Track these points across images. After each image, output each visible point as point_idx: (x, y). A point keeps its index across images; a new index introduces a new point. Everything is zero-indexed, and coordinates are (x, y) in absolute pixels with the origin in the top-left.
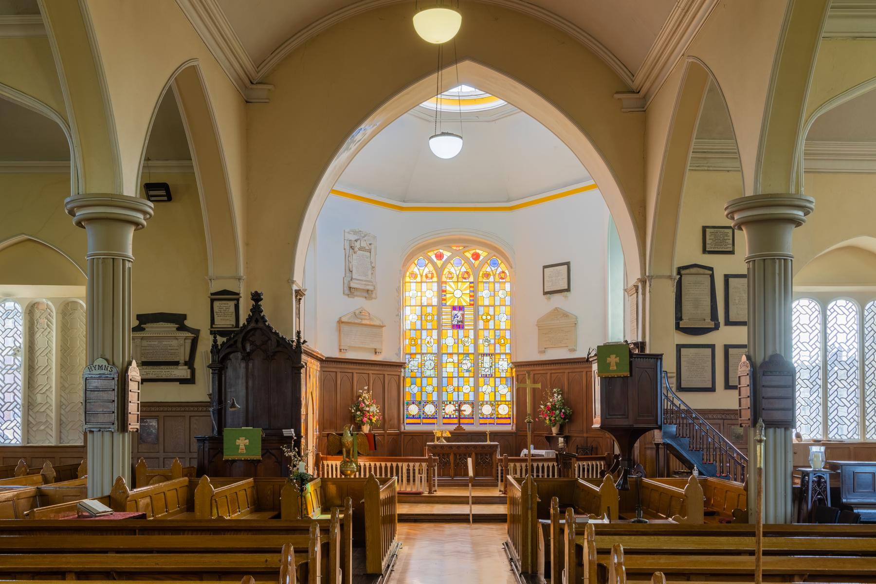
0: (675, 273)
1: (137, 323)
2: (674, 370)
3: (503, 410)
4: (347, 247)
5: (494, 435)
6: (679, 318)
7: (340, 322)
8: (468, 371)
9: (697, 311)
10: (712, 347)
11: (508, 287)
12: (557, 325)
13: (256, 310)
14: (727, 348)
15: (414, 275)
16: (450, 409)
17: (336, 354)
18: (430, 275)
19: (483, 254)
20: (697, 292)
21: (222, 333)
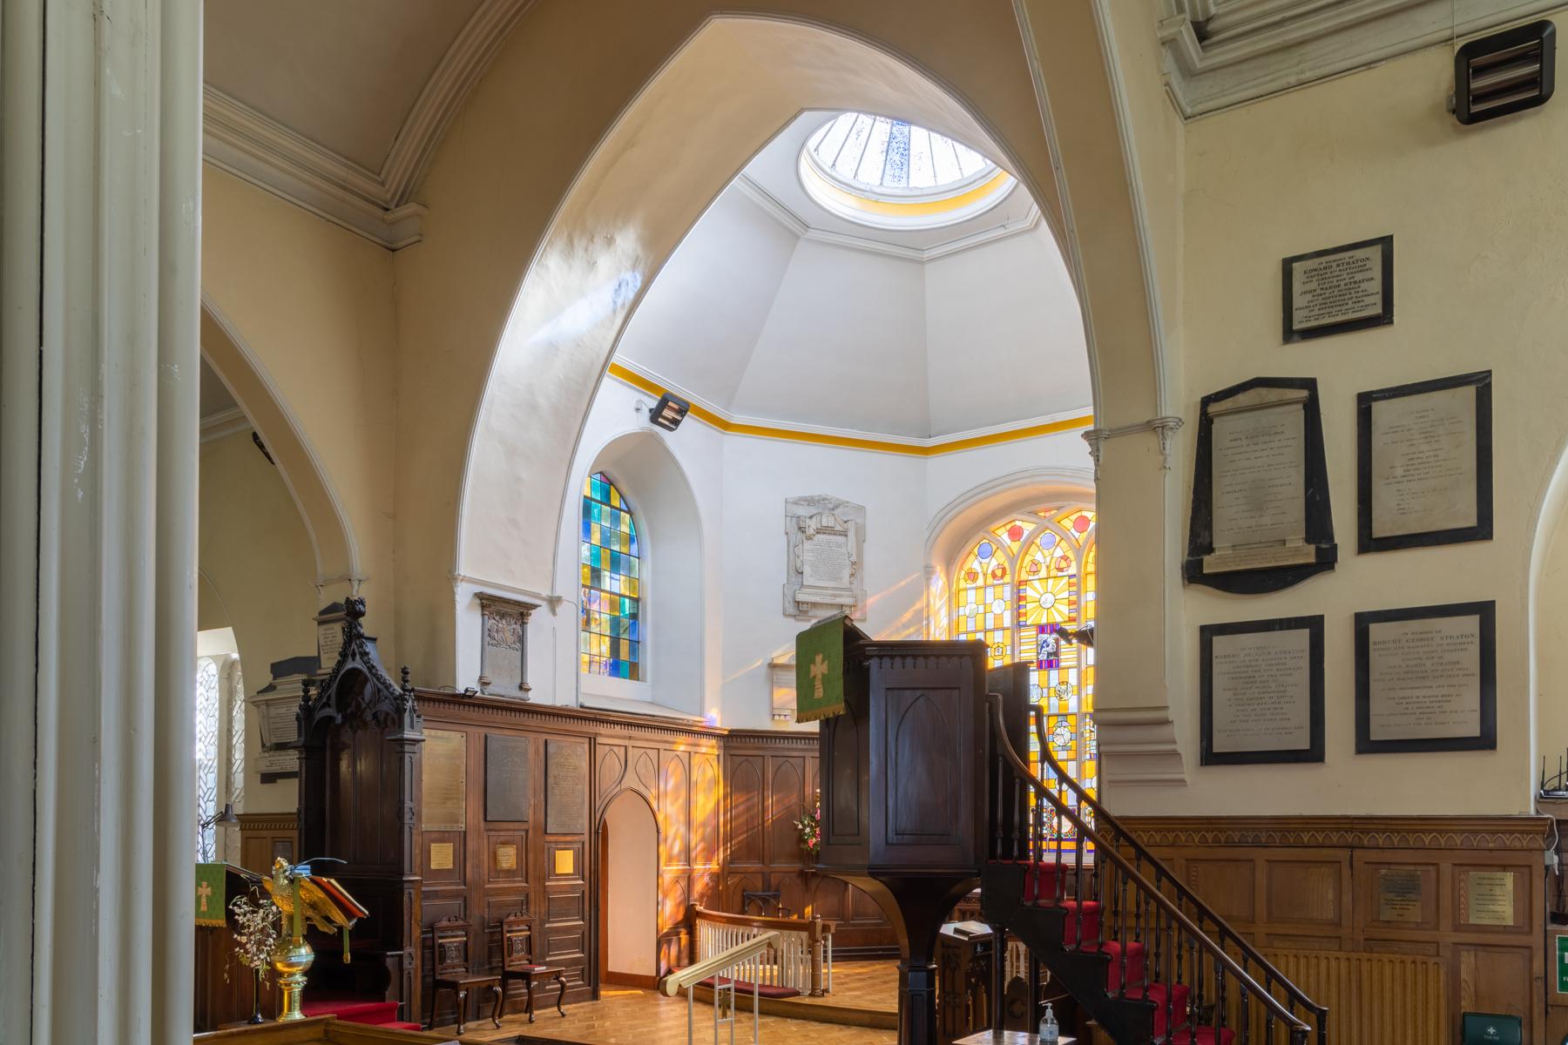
1: (269, 678)
4: (793, 530)
8: (1064, 748)
9: (1259, 519)
10: (1314, 625)
14: (1363, 622)
15: (972, 576)
18: (999, 573)
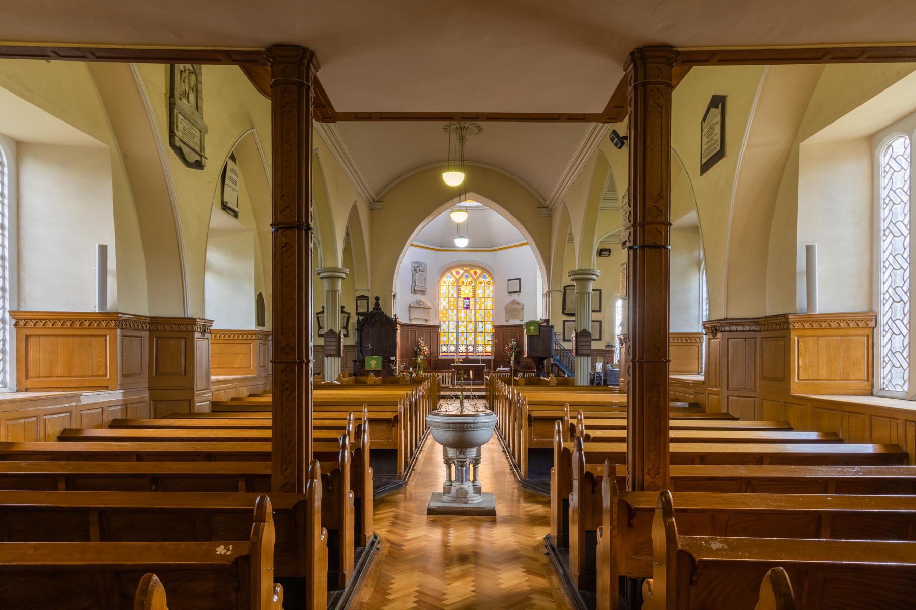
0: (562, 289)
2: (562, 331)
3: (489, 349)
5: (483, 361)
6: (564, 308)
7: (410, 307)
11: (491, 288)
12: (514, 309)
13: (377, 304)
15: (445, 282)
16: (462, 348)
17: (408, 322)
19: (479, 272)
20: (572, 297)
21: (362, 315)
